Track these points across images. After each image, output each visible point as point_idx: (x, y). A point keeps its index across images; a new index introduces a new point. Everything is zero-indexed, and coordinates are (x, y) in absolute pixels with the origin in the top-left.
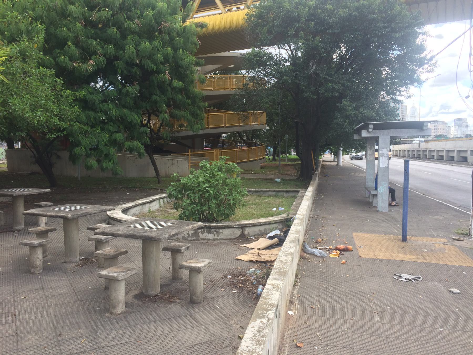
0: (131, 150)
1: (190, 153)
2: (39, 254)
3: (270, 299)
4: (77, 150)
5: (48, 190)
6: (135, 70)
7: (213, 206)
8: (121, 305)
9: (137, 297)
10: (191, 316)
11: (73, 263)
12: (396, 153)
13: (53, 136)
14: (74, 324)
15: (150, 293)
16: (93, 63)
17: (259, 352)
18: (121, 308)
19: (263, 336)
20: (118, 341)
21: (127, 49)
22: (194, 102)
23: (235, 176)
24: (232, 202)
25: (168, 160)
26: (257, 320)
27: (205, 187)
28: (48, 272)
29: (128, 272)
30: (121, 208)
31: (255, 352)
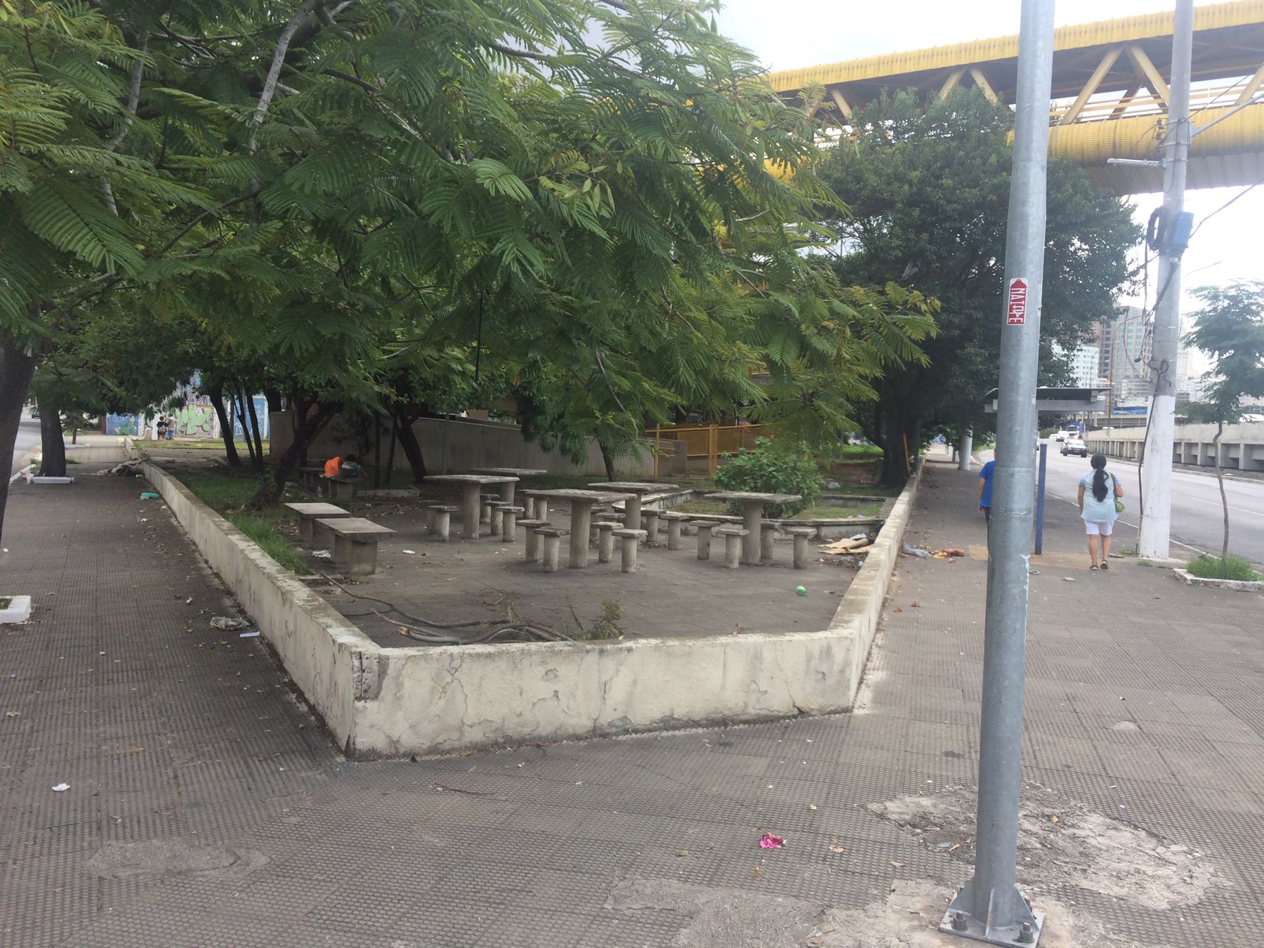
12: (1113, 450)
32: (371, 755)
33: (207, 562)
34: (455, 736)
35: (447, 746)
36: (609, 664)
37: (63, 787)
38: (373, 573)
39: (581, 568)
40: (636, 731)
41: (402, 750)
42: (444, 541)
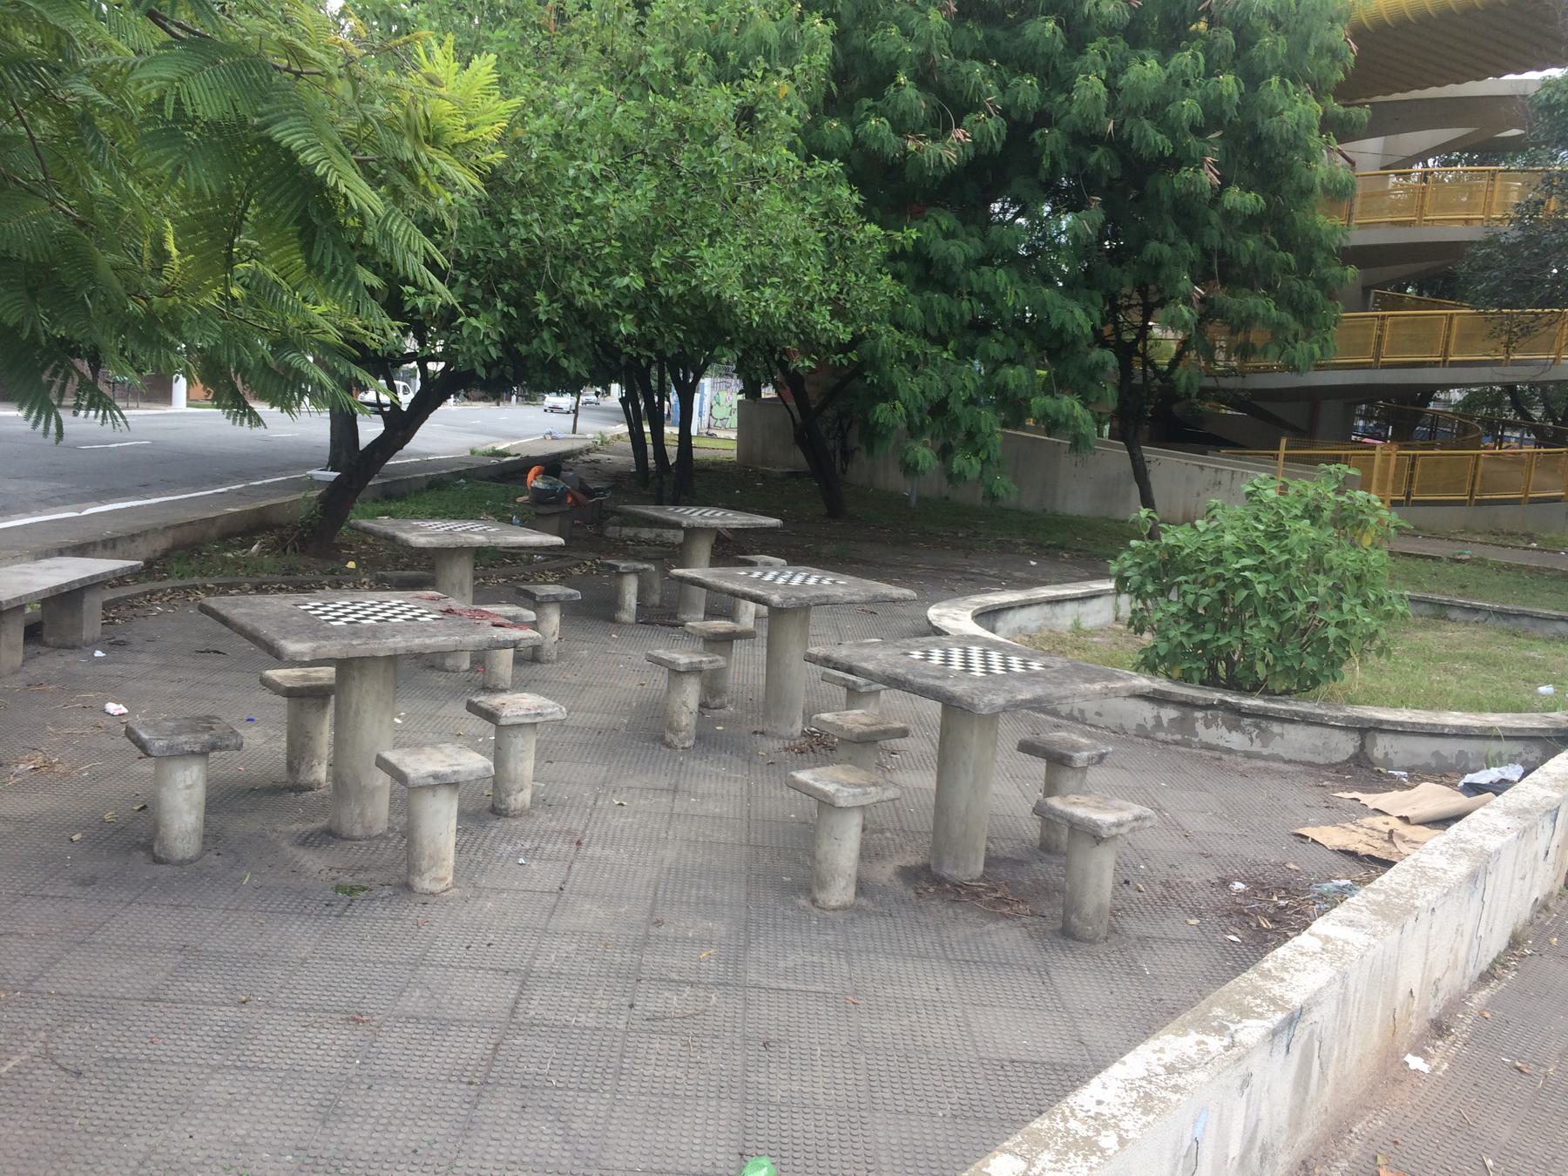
0: (1052, 424)
1: (1282, 451)
2: (691, 693)
3: (1282, 980)
4: (882, 411)
5: (774, 522)
6: (1097, 157)
7: (1257, 636)
8: (843, 884)
9: (911, 875)
10: (1044, 972)
11: (780, 737)
13: (807, 363)
14: (706, 904)
15: (949, 871)
16: (965, 136)
17: (1127, 1131)
18: (840, 892)
19: (1176, 1089)
20: (796, 981)
21: (1080, 87)
22: (1306, 264)
24: (1332, 632)
25: (1202, 468)
26: (1186, 1034)
27: (1238, 566)
28: (709, 751)
29: (873, 789)
30: (978, 604)
31: (1117, 1126)
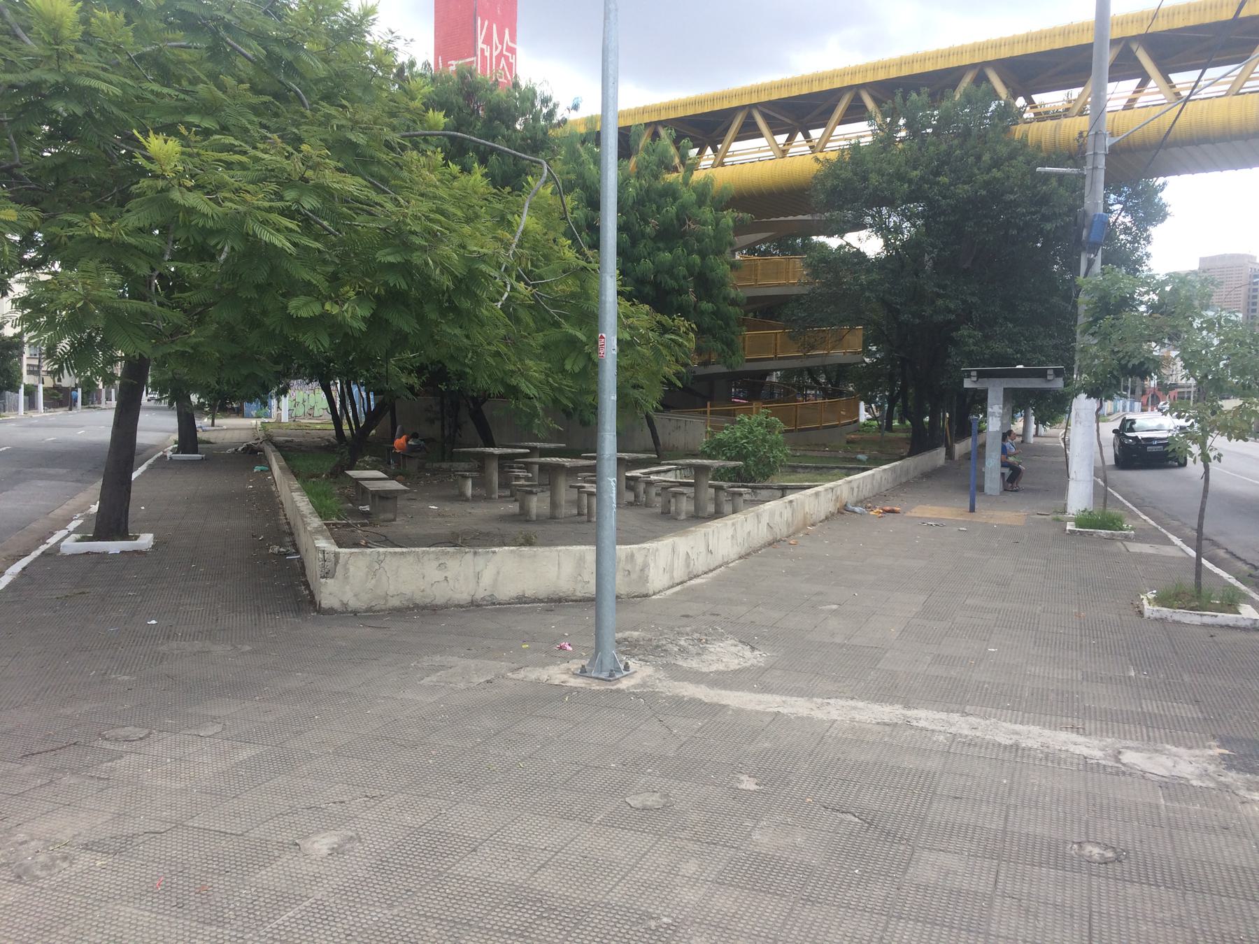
1: (709, 409)
5: (564, 445)
23: (777, 433)
32: (331, 611)
33: (285, 515)
34: (382, 602)
35: (377, 608)
36: (480, 561)
37: (154, 622)
38: (394, 520)
39: (558, 518)
40: (499, 604)
41: (350, 610)
42: (467, 500)
